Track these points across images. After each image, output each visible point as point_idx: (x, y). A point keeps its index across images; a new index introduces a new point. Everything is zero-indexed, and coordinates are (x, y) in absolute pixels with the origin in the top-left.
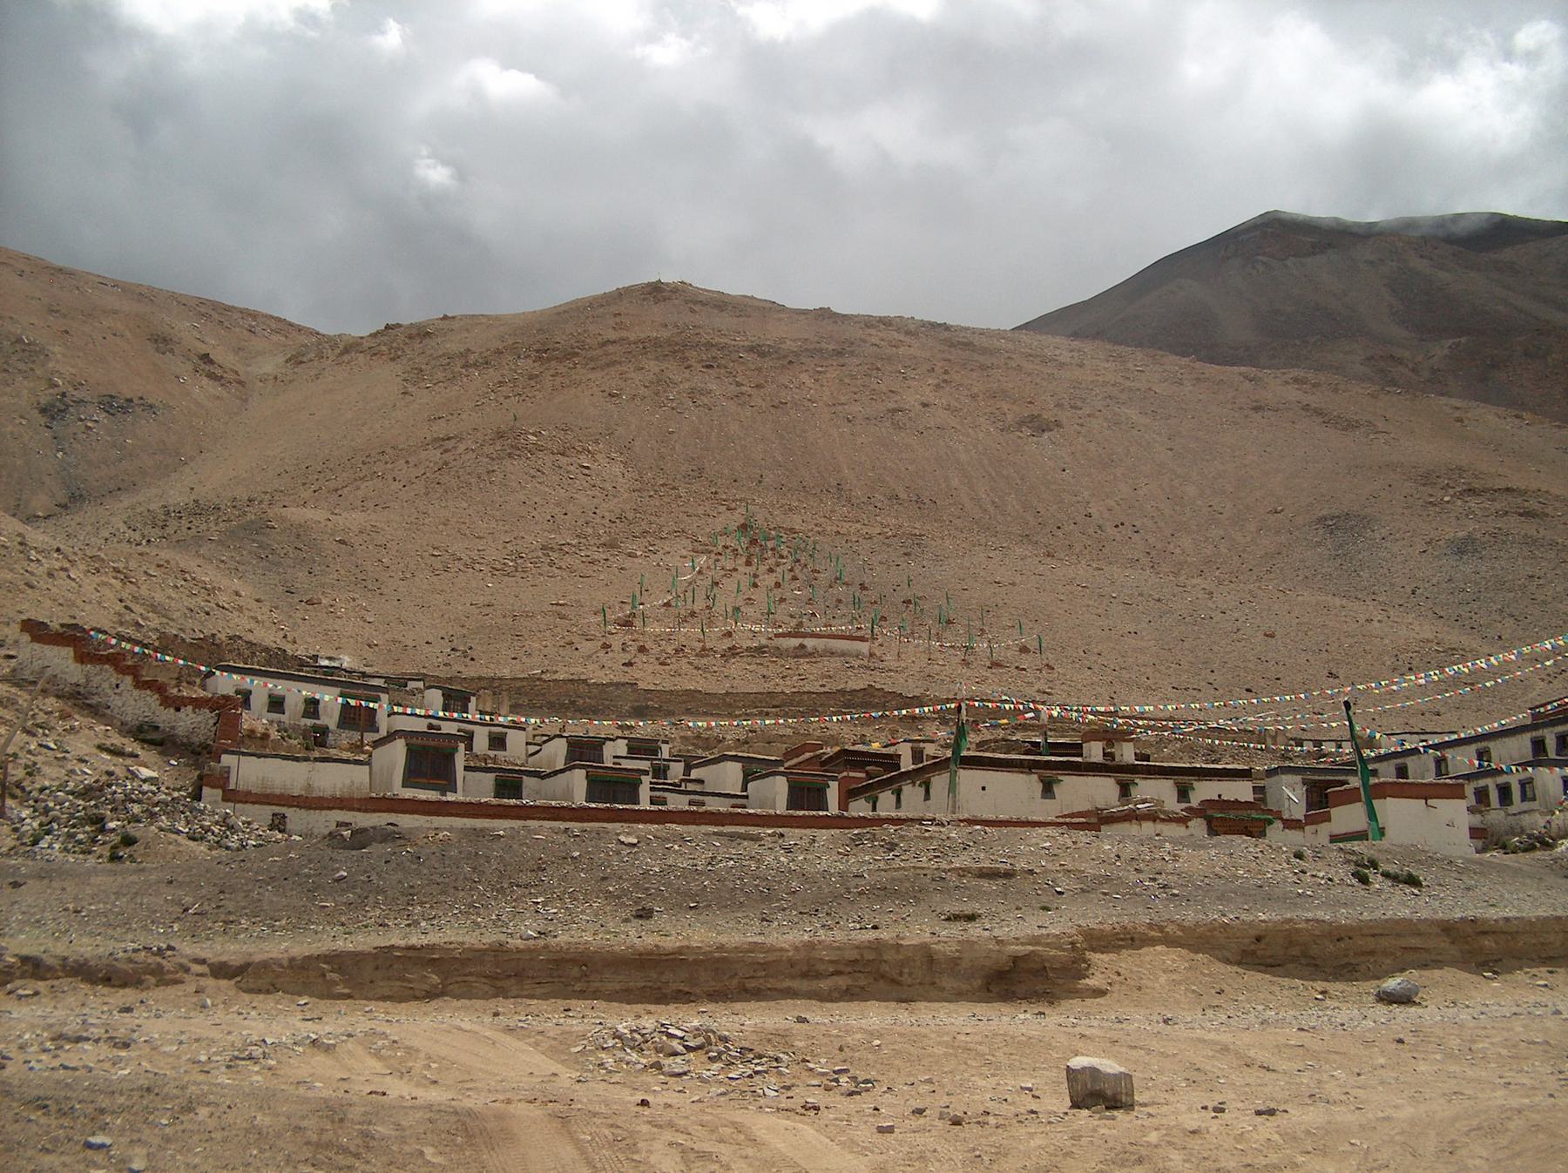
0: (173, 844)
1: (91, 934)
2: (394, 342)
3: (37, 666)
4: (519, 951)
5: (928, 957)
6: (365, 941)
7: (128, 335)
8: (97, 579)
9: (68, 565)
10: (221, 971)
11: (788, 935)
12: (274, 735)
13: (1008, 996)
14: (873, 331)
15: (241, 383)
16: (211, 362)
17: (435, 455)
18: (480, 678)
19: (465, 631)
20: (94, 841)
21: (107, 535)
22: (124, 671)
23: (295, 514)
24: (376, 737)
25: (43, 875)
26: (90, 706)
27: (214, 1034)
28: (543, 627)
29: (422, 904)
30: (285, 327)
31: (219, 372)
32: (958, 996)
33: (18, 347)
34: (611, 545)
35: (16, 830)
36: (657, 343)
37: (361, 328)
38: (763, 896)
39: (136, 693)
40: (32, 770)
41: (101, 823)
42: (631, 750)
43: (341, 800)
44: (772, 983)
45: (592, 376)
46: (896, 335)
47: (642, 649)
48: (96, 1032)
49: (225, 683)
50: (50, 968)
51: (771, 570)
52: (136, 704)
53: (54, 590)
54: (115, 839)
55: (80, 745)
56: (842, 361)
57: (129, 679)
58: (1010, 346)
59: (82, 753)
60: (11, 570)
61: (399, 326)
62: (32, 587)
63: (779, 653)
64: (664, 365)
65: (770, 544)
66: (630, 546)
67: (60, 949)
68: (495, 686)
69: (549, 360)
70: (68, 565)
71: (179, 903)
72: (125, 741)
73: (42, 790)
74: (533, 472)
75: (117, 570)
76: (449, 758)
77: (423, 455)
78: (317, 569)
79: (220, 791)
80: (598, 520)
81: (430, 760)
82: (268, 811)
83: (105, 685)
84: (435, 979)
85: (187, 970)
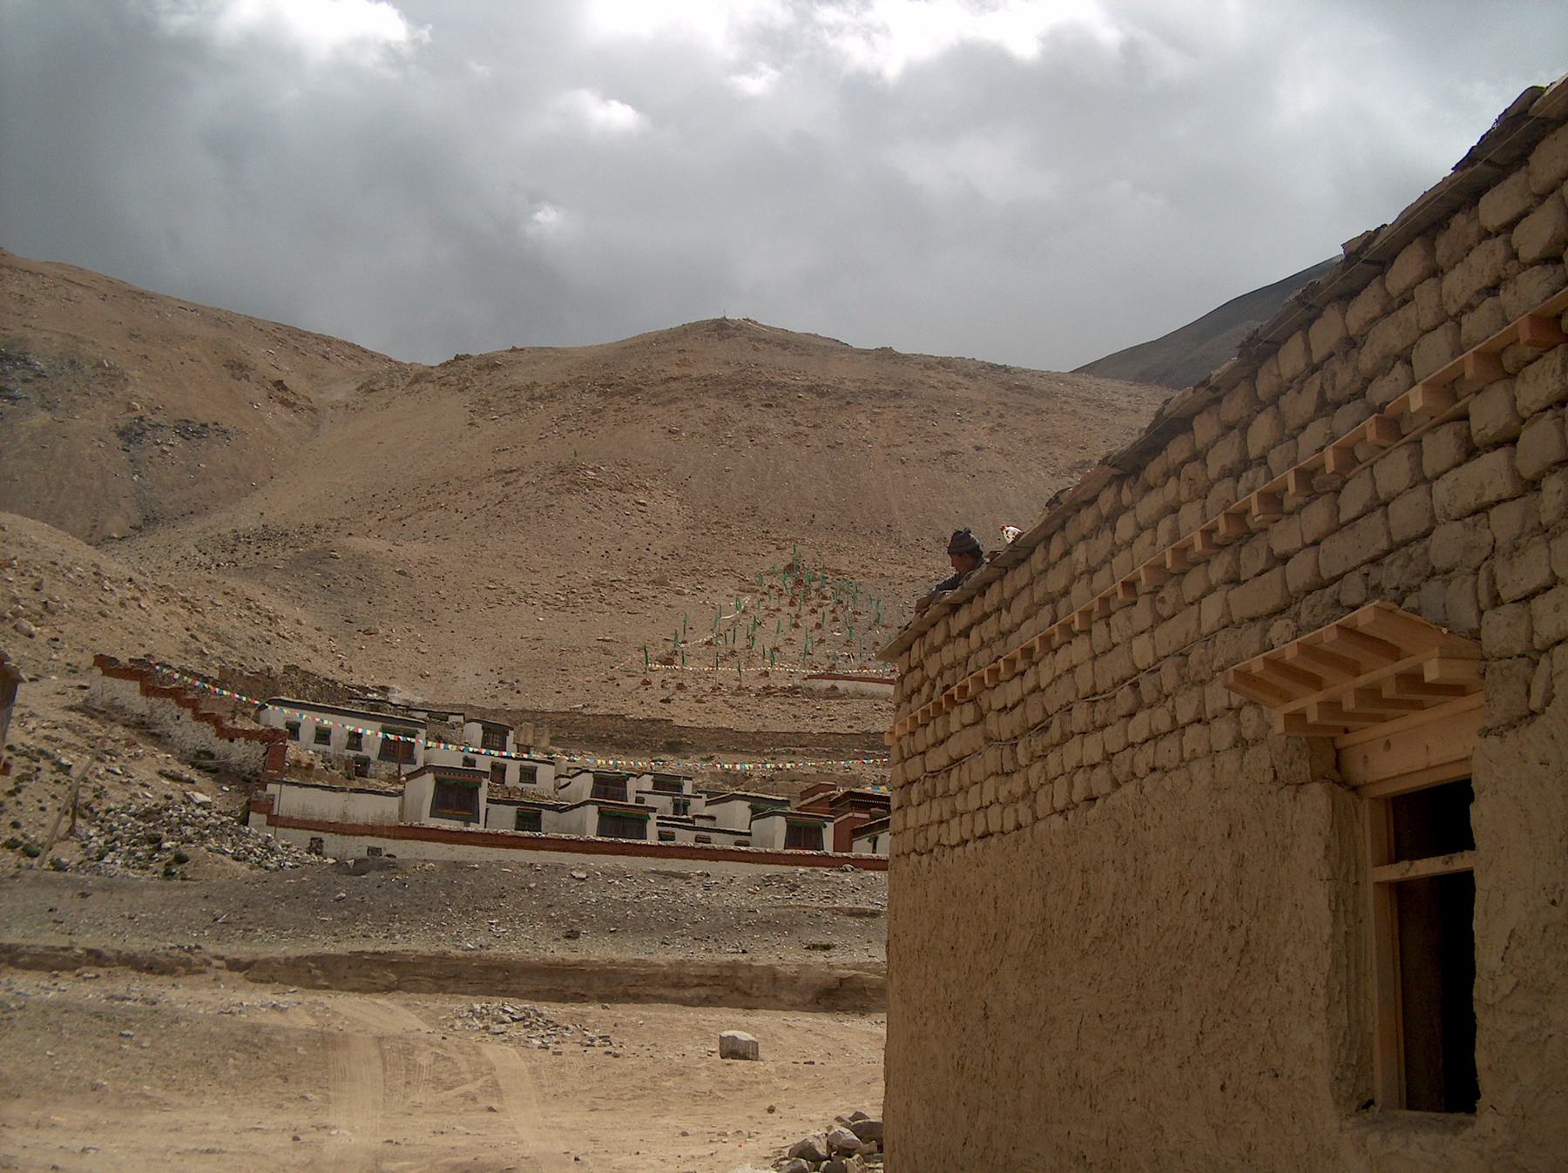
0: (219, 863)
1: (141, 936)
2: (463, 372)
3: (106, 697)
4: (458, 958)
5: (773, 975)
6: (345, 947)
7: (205, 360)
8: (166, 608)
9: (139, 595)
10: (234, 965)
11: (664, 956)
12: (319, 765)
13: (831, 1009)
14: (931, 373)
15: (313, 410)
16: (285, 389)
17: (497, 487)
18: (524, 711)
19: (513, 664)
20: (151, 858)
21: (178, 558)
22: (184, 704)
23: (360, 544)
24: (415, 768)
25: (107, 888)
26: (154, 734)
27: (212, 999)
28: (587, 662)
29: (400, 921)
30: (358, 353)
31: (292, 399)
32: (793, 1006)
33: (99, 370)
34: (661, 582)
35: (84, 846)
36: (717, 381)
37: (433, 356)
38: (669, 924)
39: (195, 724)
40: (99, 794)
41: (158, 842)
42: (657, 785)
43: (372, 827)
44: (649, 990)
45: (654, 412)
46: (954, 377)
47: (680, 687)
48: (134, 995)
49: (277, 717)
50: (108, 959)
51: (814, 611)
52: (197, 735)
53: (125, 619)
54: (170, 857)
55: (143, 771)
56: (899, 403)
57: (188, 712)
58: (1069, 390)
59: (145, 778)
60: (86, 600)
61: (468, 356)
62: (105, 616)
63: (811, 693)
64: (725, 403)
65: (815, 585)
66: (679, 584)
67: (117, 945)
68: (536, 718)
69: (613, 395)
70: (139, 595)
71: (211, 914)
72: (183, 767)
73: (108, 811)
74: (590, 507)
75: (184, 600)
76: (474, 791)
77: (486, 487)
78: (376, 599)
79: (264, 817)
80: (651, 556)
81: (456, 793)
82: (305, 836)
83: (168, 717)
84: (393, 977)
85: (209, 964)
